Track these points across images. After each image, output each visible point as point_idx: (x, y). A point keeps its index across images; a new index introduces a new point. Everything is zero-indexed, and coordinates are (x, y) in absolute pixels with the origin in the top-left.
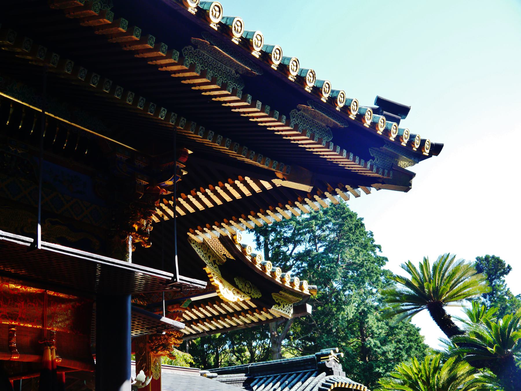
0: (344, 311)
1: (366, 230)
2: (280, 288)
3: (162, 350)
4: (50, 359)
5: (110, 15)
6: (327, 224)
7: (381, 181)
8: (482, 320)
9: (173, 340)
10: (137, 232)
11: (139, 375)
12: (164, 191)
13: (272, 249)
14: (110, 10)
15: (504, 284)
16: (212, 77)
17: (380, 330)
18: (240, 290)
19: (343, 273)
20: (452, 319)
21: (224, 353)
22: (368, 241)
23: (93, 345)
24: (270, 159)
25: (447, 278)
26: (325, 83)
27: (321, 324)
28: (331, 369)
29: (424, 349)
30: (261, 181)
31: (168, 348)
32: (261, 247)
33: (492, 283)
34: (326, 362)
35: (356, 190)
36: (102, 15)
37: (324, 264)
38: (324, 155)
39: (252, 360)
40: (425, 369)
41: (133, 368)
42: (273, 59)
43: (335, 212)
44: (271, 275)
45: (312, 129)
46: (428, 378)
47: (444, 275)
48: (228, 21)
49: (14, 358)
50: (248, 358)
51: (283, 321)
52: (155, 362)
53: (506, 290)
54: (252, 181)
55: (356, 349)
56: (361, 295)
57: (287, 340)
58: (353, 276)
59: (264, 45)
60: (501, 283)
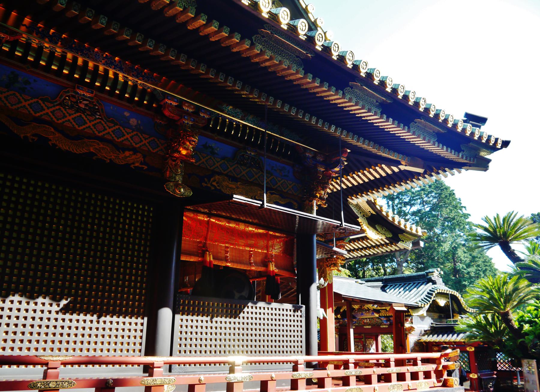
1: (456, 197)
2: (403, 231)
6: (431, 193)
7: (468, 165)
8: (536, 253)
10: (319, 198)
16: (362, 105)
17: (466, 259)
18: (379, 232)
20: (516, 252)
23: (295, 263)
27: (428, 254)
28: (435, 281)
34: (432, 277)
35: (452, 171)
36: (297, 72)
37: (429, 218)
38: (431, 150)
39: (385, 274)
40: (497, 283)
41: (317, 277)
46: (499, 289)
47: (510, 224)
51: (404, 251)
55: (450, 270)
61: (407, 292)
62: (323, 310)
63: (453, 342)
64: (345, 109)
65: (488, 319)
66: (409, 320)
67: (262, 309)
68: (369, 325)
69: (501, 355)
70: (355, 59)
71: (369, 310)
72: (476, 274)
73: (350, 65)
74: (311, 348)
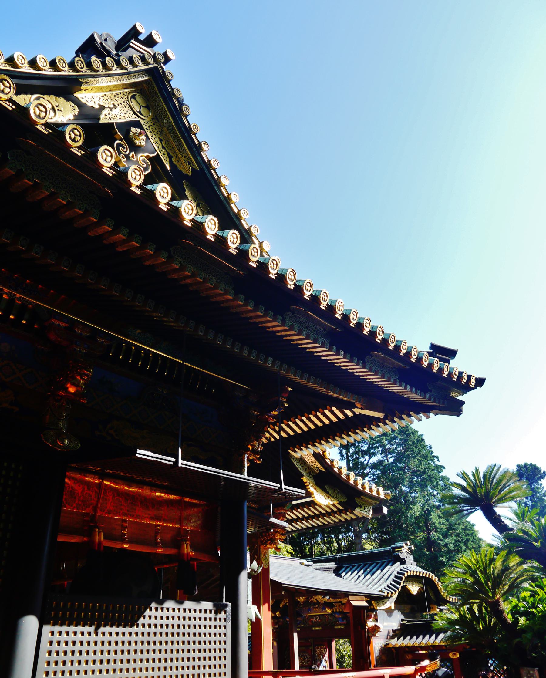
0: (412, 510)
1: (426, 444)
2: (361, 493)
3: (270, 544)
4: (186, 552)
5: (82, 206)
6: (395, 439)
8: (526, 519)
9: (278, 536)
11: (252, 564)
12: (271, 419)
13: (352, 460)
14: (232, 289)
15: (542, 487)
16: (306, 334)
17: (442, 526)
18: (330, 495)
19: (409, 479)
20: (501, 518)
21: (317, 544)
22: (428, 453)
24: (351, 394)
25: (495, 484)
26: (391, 335)
27: (394, 520)
28: (404, 559)
29: (479, 542)
30: (344, 410)
31: (275, 542)
32: (344, 459)
33: (531, 486)
34: (400, 553)
35: (418, 416)
36: (226, 293)
37: (393, 472)
38: (392, 390)
41: (248, 557)
42: (365, 327)
43: (401, 430)
44: (354, 483)
45: (382, 370)
46: (485, 568)
47: (492, 481)
48: (317, 293)
49: (159, 551)
50: (336, 548)
51: (364, 519)
52: (264, 554)
53: (544, 492)
54: (337, 410)
55: (423, 542)
56: (425, 497)
57: (367, 534)
58: (418, 481)
59: (344, 310)
60: (539, 486)
61: (369, 576)
62: (255, 608)
63: (431, 646)
64: (285, 338)
65: (474, 611)
66: (373, 616)
67: (171, 610)
68: (318, 626)
69: (494, 662)
70: (298, 279)
71: (318, 603)
72: (455, 546)
73: (291, 285)
74: (238, 671)
